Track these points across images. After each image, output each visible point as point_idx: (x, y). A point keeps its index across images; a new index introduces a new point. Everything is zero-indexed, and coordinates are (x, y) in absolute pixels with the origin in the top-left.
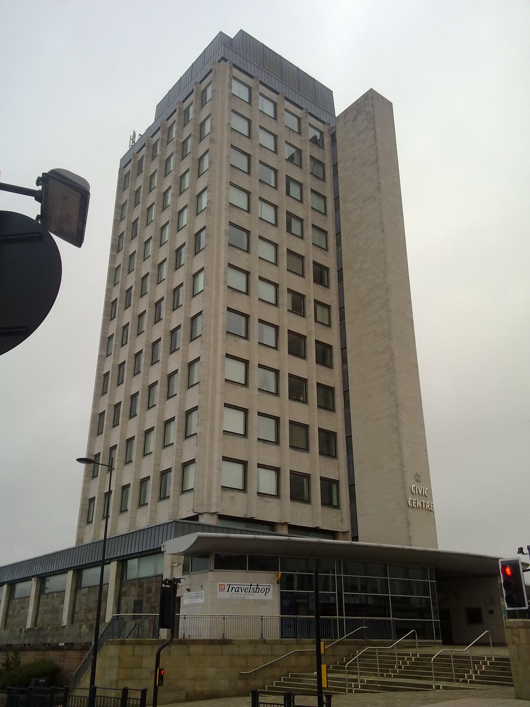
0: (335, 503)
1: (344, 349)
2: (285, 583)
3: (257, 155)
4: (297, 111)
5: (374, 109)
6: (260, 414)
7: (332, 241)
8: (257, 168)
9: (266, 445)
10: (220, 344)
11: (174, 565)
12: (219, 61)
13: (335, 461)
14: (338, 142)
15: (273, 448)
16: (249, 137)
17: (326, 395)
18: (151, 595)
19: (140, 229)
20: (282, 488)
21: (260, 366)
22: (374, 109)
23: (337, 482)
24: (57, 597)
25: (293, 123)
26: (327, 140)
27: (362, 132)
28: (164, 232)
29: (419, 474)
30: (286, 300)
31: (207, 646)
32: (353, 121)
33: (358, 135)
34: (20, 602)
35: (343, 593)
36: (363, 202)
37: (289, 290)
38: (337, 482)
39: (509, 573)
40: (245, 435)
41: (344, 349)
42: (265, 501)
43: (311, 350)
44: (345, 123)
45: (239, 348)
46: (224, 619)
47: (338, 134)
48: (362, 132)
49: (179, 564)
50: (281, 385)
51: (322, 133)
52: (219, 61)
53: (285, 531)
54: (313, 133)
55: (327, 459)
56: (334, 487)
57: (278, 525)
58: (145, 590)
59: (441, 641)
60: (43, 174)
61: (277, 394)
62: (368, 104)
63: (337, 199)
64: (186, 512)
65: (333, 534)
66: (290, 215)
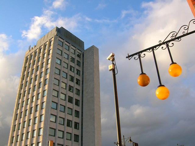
0: (78, 128)
1: (82, 113)
3: (63, 60)
4: (74, 48)
5: (93, 49)
6: (59, 130)
7: (81, 64)
8: (63, 63)
9: (60, 139)
10: (53, 76)
13: (78, 143)
14: (84, 57)
15: (62, 139)
16: (61, 55)
17: (78, 81)
20: (66, 98)
21: (59, 117)
22: (93, 49)
23: (78, 123)
25: (73, 51)
26: (82, 56)
30: (69, 78)
37: (70, 75)
38: (79, 101)
40: (55, 122)
41: (82, 113)
43: (74, 101)
45: (55, 112)
47: (84, 55)
50: (65, 122)
51: (80, 54)
54: (77, 53)
55: (76, 142)
56: (78, 124)
60: (6, 53)
61: (63, 125)
63: (83, 72)
66: (71, 67)
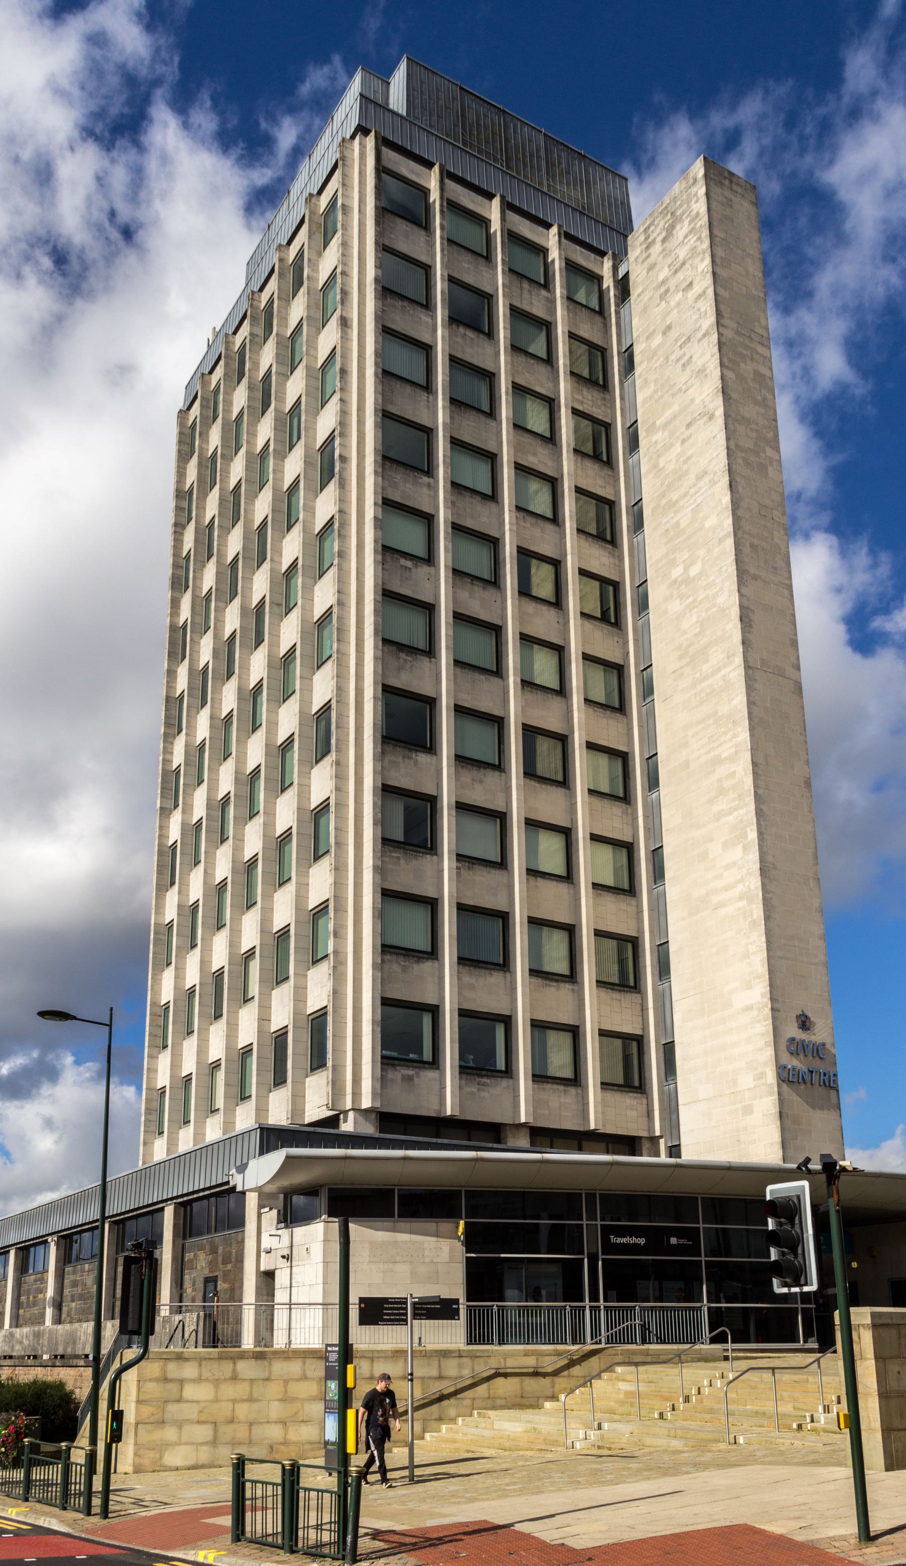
2: (471, 1241)
11: (262, 1211)
12: (353, 137)
18: (229, 1267)
19: (306, 420)
24: (89, 1271)
27: (683, 264)
28: (293, 500)
29: (806, 1013)
31: (308, 1361)
32: (664, 241)
33: (676, 272)
34: (36, 1281)
35: (600, 1256)
36: (689, 425)
39: (770, 1220)
42: (479, 1084)
44: (647, 248)
46: (290, 1309)
47: (637, 350)
48: (683, 264)
49: (271, 1209)
52: (353, 137)
53: (524, 1141)
57: (508, 1128)
58: (220, 1259)
59: (816, 1346)
62: (696, 194)
64: (315, 1109)
65: (630, 1144)
